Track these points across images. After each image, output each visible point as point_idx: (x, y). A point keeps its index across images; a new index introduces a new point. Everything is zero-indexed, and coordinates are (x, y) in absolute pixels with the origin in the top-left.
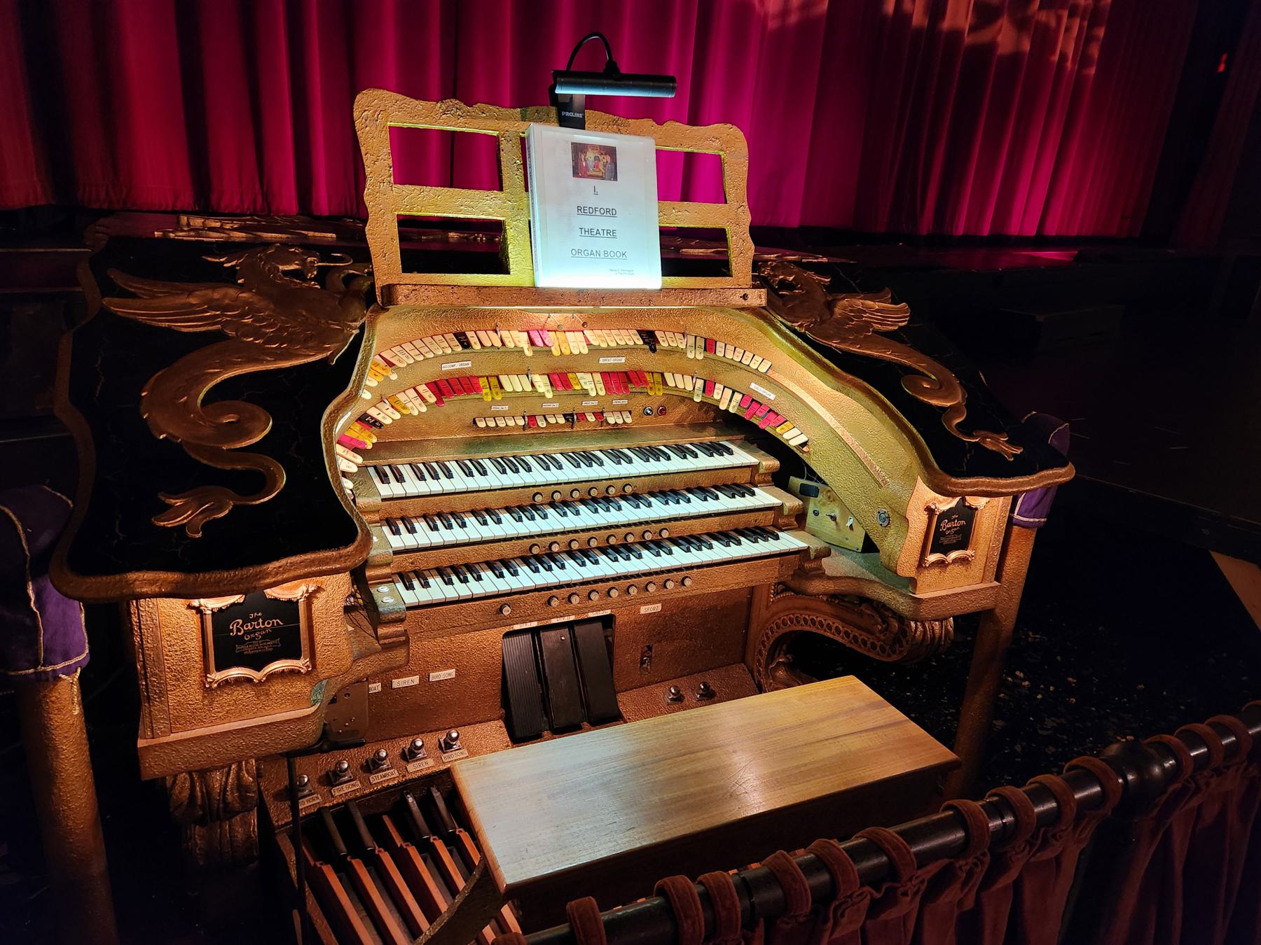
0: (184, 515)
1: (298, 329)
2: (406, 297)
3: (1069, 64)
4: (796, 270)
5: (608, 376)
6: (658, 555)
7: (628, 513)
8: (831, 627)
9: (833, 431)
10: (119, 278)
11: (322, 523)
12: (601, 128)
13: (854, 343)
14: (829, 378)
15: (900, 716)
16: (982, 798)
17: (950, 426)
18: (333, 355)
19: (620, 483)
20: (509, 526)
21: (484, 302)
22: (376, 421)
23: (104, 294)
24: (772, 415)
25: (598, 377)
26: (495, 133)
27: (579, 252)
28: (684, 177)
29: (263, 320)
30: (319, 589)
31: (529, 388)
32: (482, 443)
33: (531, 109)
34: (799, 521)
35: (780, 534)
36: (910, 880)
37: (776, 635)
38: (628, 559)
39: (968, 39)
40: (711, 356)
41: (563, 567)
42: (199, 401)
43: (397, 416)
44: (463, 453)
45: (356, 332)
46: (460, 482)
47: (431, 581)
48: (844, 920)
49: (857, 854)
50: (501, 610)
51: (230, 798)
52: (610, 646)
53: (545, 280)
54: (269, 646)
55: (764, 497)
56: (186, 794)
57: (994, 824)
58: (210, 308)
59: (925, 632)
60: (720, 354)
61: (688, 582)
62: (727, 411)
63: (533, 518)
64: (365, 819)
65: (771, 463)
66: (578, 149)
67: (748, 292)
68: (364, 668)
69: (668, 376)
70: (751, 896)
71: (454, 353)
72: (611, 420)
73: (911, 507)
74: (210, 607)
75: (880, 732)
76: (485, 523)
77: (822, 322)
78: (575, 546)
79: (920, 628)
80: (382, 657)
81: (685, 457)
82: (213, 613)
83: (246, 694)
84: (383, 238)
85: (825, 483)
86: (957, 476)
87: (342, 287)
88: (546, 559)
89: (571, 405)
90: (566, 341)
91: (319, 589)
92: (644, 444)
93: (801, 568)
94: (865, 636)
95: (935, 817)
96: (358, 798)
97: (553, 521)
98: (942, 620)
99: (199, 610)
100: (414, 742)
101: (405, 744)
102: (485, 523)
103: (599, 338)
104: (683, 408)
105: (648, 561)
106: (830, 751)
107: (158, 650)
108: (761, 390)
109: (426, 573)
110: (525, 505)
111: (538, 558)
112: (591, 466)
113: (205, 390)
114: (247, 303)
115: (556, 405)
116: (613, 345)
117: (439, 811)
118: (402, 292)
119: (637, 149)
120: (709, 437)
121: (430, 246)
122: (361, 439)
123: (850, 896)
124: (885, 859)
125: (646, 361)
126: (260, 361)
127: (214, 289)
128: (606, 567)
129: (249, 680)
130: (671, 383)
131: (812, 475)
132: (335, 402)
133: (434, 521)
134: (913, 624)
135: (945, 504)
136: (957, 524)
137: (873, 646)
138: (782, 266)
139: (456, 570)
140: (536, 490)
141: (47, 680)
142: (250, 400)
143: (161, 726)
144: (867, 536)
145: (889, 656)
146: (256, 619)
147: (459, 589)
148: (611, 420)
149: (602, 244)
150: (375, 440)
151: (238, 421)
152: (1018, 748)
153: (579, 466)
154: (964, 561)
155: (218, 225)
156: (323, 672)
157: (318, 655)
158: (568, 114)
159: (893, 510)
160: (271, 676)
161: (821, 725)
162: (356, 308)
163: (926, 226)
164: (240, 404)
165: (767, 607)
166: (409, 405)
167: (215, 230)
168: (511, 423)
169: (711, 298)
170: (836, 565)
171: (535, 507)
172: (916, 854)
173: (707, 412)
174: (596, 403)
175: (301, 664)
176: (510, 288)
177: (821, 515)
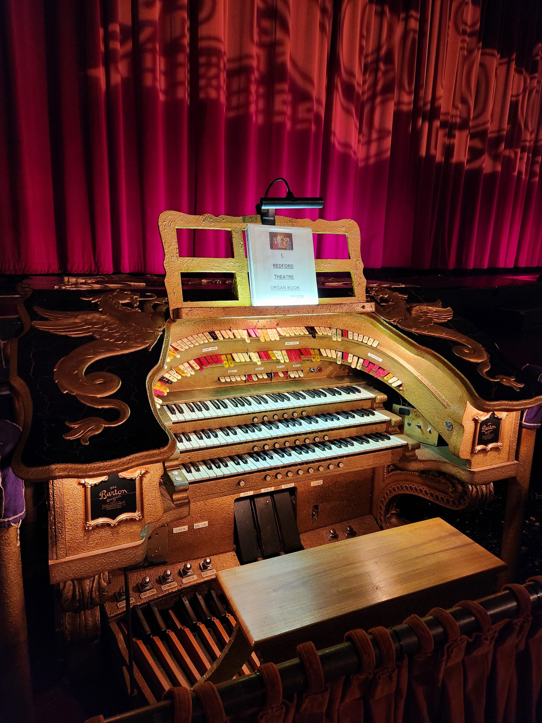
0: (81, 432)
1: (132, 333)
2: (187, 314)
3: (523, 177)
4: (389, 292)
5: (291, 352)
6: (324, 450)
7: (305, 427)
8: (421, 490)
9: (416, 378)
10: (40, 311)
11: (147, 435)
12: (282, 224)
13: (424, 329)
14: (413, 349)
15: (469, 540)
16: (524, 583)
17: (482, 373)
18: (150, 346)
19: (300, 410)
20: (241, 436)
21: (226, 315)
22: (169, 380)
23: (32, 319)
24: (381, 371)
25: (284, 352)
26: (230, 230)
27: (275, 287)
28: (324, 247)
29: (113, 329)
30: (147, 472)
31: (248, 360)
32: (223, 391)
33: (247, 217)
34: (400, 429)
35: (391, 436)
36: (488, 631)
37: (390, 497)
38: (308, 452)
39: (467, 167)
40: (345, 339)
41: (272, 458)
42: (83, 373)
43: (180, 377)
44: (213, 396)
45: (161, 333)
46: (213, 412)
47: (200, 468)
48: (453, 654)
49: (458, 616)
50: (239, 484)
51: (94, 595)
52: (294, 506)
53: (257, 302)
54: (119, 505)
55: (380, 416)
56: (70, 593)
57: (533, 597)
58: (86, 324)
59: (477, 492)
60: (350, 337)
61: (341, 465)
62: (356, 369)
63: (254, 431)
64: (160, 612)
65: (382, 397)
66: (273, 235)
67: (365, 304)
68: (168, 517)
69: (322, 351)
70: (400, 641)
71: (209, 343)
72: (292, 376)
73: (465, 418)
74: (90, 483)
75: (459, 550)
76: (228, 435)
77: (406, 319)
78: (277, 446)
79: (475, 489)
80: (176, 512)
81: (334, 395)
82: (92, 487)
83: (105, 533)
84: (174, 286)
85: (413, 407)
86: (490, 400)
87: (152, 310)
88: (262, 454)
89: (271, 368)
90: (267, 334)
91: (147, 472)
92: (311, 388)
93: (404, 455)
94: (442, 495)
95: (499, 594)
96: (155, 599)
97: (265, 433)
98: (487, 484)
99: (84, 485)
100: (186, 565)
101: (181, 566)
102: (228, 435)
103: (285, 331)
104: (331, 368)
105: (319, 454)
106: (430, 561)
107: (62, 508)
108: (374, 357)
109: (197, 463)
110: (249, 424)
111: (258, 454)
112: (283, 401)
113: (86, 367)
114: (105, 321)
115: (263, 368)
116: (293, 335)
117: (213, 600)
118: (184, 312)
119: (303, 234)
120: (346, 383)
121: (200, 288)
122: (161, 390)
123: (456, 641)
124: (473, 618)
125: (311, 343)
126: (113, 351)
127: (88, 314)
128: (295, 457)
129: (108, 525)
130: (324, 355)
131: (405, 402)
132: (152, 371)
133: (200, 435)
134: (470, 487)
135: (484, 417)
136: (491, 428)
137: (448, 501)
138: (381, 290)
139: (213, 461)
140: (254, 415)
141: (5, 527)
142: (109, 371)
143: (61, 552)
144: (439, 435)
145: (458, 507)
146: (113, 490)
147: (215, 472)
148: (292, 376)
149: (287, 282)
150: (168, 391)
151: (104, 383)
152: (537, 563)
153: (277, 401)
154: (496, 449)
155: (84, 281)
156: (148, 519)
157: (145, 510)
158: (266, 218)
159: (455, 421)
160: (121, 522)
161: (424, 547)
162: (160, 321)
163: (452, 264)
164: (104, 373)
165: (383, 481)
166: (185, 371)
167: (84, 284)
168: (239, 379)
169: (345, 309)
170: (422, 453)
171: (254, 425)
172: (492, 615)
173: (344, 370)
174: (283, 366)
175: (136, 515)
176: (240, 307)
177: (412, 425)
